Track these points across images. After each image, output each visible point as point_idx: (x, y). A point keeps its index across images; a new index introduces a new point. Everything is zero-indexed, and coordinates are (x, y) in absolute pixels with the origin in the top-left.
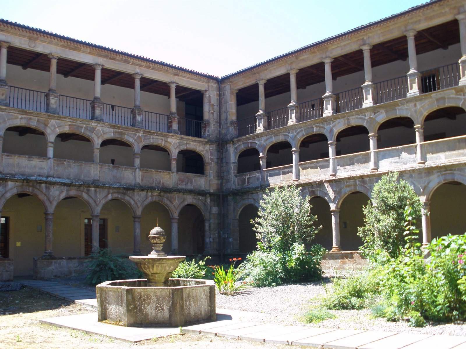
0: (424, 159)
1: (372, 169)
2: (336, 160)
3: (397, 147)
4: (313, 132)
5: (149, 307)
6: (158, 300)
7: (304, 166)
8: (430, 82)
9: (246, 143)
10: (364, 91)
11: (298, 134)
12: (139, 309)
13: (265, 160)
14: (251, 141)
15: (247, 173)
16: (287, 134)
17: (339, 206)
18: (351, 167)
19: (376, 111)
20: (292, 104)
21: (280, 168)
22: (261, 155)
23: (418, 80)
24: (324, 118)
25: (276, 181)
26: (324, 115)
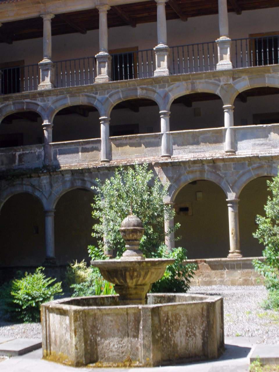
0: (170, 151)
1: (227, 152)
2: (171, 136)
3: (265, 125)
4: (137, 96)
5: (178, 333)
6: (188, 322)
7: (118, 142)
8: (121, 67)
9: (18, 103)
10: (218, 48)
11: (111, 96)
12: (166, 338)
13: (50, 130)
14: (28, 100)
15: (19, 147)
16: (94, 95)
17: (174, 200)
18: (195, 147)
19: (237, 76)
20: (46, 61)
21: (79, 142)
22: (46, 122)
23: (168, 57)
24: (157, 78)
25: (71, 160)
26: (156, 75)
